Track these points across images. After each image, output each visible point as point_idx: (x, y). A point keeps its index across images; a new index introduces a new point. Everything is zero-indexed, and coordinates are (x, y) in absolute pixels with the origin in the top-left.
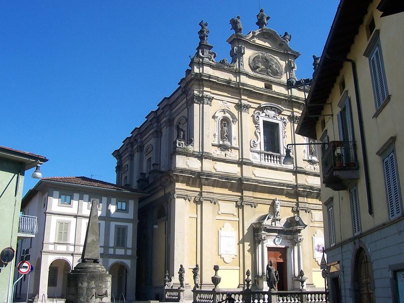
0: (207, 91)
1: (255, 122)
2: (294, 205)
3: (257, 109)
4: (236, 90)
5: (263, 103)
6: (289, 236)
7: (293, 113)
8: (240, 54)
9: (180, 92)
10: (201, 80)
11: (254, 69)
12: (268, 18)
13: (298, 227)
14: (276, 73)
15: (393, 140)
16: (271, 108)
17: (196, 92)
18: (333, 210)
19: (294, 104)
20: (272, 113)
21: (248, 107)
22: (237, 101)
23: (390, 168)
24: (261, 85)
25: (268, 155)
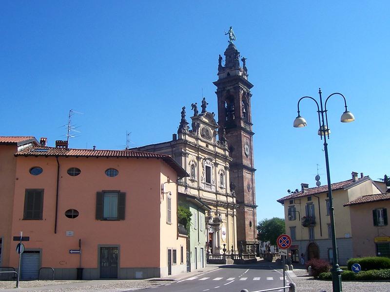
0: (188, 150)
1: (203, 167)
2: (226, 212)
3: (204, 159)
4: (197, 149)
5: (207, 156)
6: (214, 227)
7: (216, 161)
8: (198, 126)
9: (169, 144)
10: (186, 143)
11: (203, 136)
12: (208, 104)
13: (220, 223)
14: (210, 138)
15: (278, 201)
16: (209, 159)
17: (183, 150)
18: (20, 143)
19: (217, 156)
20: (208, 161)
21: (201, 158)
22: (197, 155)
23: (338, 250)
24: (204, 145)
25: (207, 184)
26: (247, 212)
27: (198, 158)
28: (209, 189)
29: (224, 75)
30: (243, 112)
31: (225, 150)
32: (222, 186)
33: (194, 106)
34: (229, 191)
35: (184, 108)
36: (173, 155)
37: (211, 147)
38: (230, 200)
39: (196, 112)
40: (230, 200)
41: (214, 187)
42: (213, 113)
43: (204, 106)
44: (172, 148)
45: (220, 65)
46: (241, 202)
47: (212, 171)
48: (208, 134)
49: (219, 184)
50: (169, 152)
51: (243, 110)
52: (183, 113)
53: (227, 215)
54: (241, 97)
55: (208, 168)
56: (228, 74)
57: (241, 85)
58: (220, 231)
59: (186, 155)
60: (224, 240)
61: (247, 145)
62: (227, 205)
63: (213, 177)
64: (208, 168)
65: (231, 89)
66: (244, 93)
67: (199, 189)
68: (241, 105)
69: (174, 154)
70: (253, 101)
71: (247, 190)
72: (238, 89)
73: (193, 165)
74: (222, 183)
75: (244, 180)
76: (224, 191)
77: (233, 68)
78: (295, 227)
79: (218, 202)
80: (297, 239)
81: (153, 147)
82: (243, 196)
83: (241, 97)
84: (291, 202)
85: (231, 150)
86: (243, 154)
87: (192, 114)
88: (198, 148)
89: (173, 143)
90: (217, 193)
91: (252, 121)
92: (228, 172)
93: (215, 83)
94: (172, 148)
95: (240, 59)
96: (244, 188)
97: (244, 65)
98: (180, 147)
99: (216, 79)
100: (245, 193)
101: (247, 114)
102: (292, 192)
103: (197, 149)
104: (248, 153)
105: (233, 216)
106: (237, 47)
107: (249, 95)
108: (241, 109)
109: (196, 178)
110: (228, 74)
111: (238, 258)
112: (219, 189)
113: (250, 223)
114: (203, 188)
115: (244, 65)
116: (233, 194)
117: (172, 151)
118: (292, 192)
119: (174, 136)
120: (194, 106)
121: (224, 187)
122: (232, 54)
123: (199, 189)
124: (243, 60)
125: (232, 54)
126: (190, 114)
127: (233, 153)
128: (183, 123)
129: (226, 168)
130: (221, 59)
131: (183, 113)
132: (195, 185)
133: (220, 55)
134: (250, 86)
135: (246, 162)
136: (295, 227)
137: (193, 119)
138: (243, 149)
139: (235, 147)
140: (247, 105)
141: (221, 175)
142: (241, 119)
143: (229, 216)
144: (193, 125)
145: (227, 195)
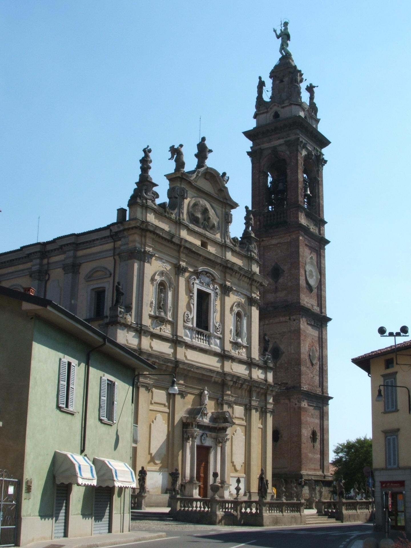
6: (214, 434)
9: (107, 233)
11: (194, 220)
13: (227, 424)
26: (305, 410)
27: (179, 270)
28: (202, 344)
29: (268, 117)
30: (306, 195)
31: (250, 259)
32: (239, 340)
33: (176, 153)
34: (255, 354)
35: (147, 151)
36: (117, 257)
37: (211, 249)
38: (258, 374)
39: (180, 164)
40: (258, 374)
41: (218, 341)
42: (224, 174)
43: (203, 151)
44: (115, 241)
45: (260, 98)
46: (293, 391)
47: (215, 304)
48: (207, 219)
49: (229, 337)
50: (107, 251)
51: (306, 191)
52: (145, 164)
53: (248, 409)
54: (301, 162)
55: (203, 298)
56: (276, 115)
57: (303, 139)
58: (228, 444)
59: (144, 257)
60: (238, 467)
61: (312, 263)
62: (249, 387)
63: (214, 318)
64: (203, 298)
65: (280, 145)
66: (309, 154)
67: (176, 342)
68: (301, 179)
69: (119, 254)
70: (329, 175)
71: (308, 361)
72: (294, 146)
73: (162, 284)
74: (238, 334)
75: (302, 338)
76: (243, 354)
77: (286, 103)
78: (398, 430)
79: (224, 374)
80: (402, 464)
81: (72, 240)
82: (299, 374)
83: (301, 162)
84: (389, 363)
85: (275, 273)
86: (302, 282)
87: (171, 167)
88: (180, 246)
89: (115, 229)
90: (223, 356)
91: (326, 217)
92: (255, 313)
93: (248, 134)
94: (115, 241)
95: (303, 86)
96: (302, 356)
97: (312, 98)
98: (131, 238)
99: (252, 124)
100: (303, 369)
101: (390, 347)
102: (391, 334)
103: (173, 245)
104: (313, 282)
105: (263, 412)
106: (299, 61)
107: (321, 161)
108: (300, 185)
109: (169, 314)
110: (276, 115)
111: (206, 509)
112: (228, 347)
113: (314, 433)
114: (188, 340)
115: (312, 98)
116: (265, 362)
117: (114, 248)
118: (391, 334)
119: (121, 212)
120: (176, 153)
121: (245, 344)
122: (286, 74)
123: (176, 342)
124: (310, 89)
125: (286, 74)
126: (161, 171)
127: (281, 280)
128: (145, 184)
129: (251, 301)
130: (261, 84)
131: (145, 164)
132: (167, 331)
133: (260, 78)
134: (324, 142)
135: (308, 301)
136: (398, 430)
137: (170, 178)
138: (302, 271)
139: (285, 268)
140: (315, 182)
141: (238, 315)
142: (299, 208)
143: (253, 411)
144: (171, 193)
145: (250, 364)
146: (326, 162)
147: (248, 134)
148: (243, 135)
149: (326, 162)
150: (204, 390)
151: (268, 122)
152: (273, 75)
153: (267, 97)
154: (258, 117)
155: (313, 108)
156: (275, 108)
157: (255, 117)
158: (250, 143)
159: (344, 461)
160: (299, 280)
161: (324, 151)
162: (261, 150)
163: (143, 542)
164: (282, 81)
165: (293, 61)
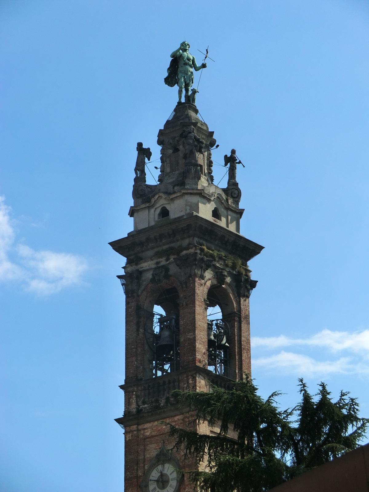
29: (150, 217)
45: (140, 178)
93: (118, 246)
95: (218, 156)
99: (125, 227)
122: (185, 138)
130: (144, 153)
146: (253, 284)
147: (118, 246)
148: (110, 248)
149: (253, 284)
150: (147, 404)
151: (153, 223)
152: (163, 138)
153: (152, 177)
154: (135, 214)
155: (233, 191)
156: (162, 202)
157: (132, 213)
158: (123, 260)
159: (316, 407)
160: (235, 353)
161: (252, 264)
162: (140, 273)
163: (174, 348)
164: (176, 150)
165: (196, 111)
